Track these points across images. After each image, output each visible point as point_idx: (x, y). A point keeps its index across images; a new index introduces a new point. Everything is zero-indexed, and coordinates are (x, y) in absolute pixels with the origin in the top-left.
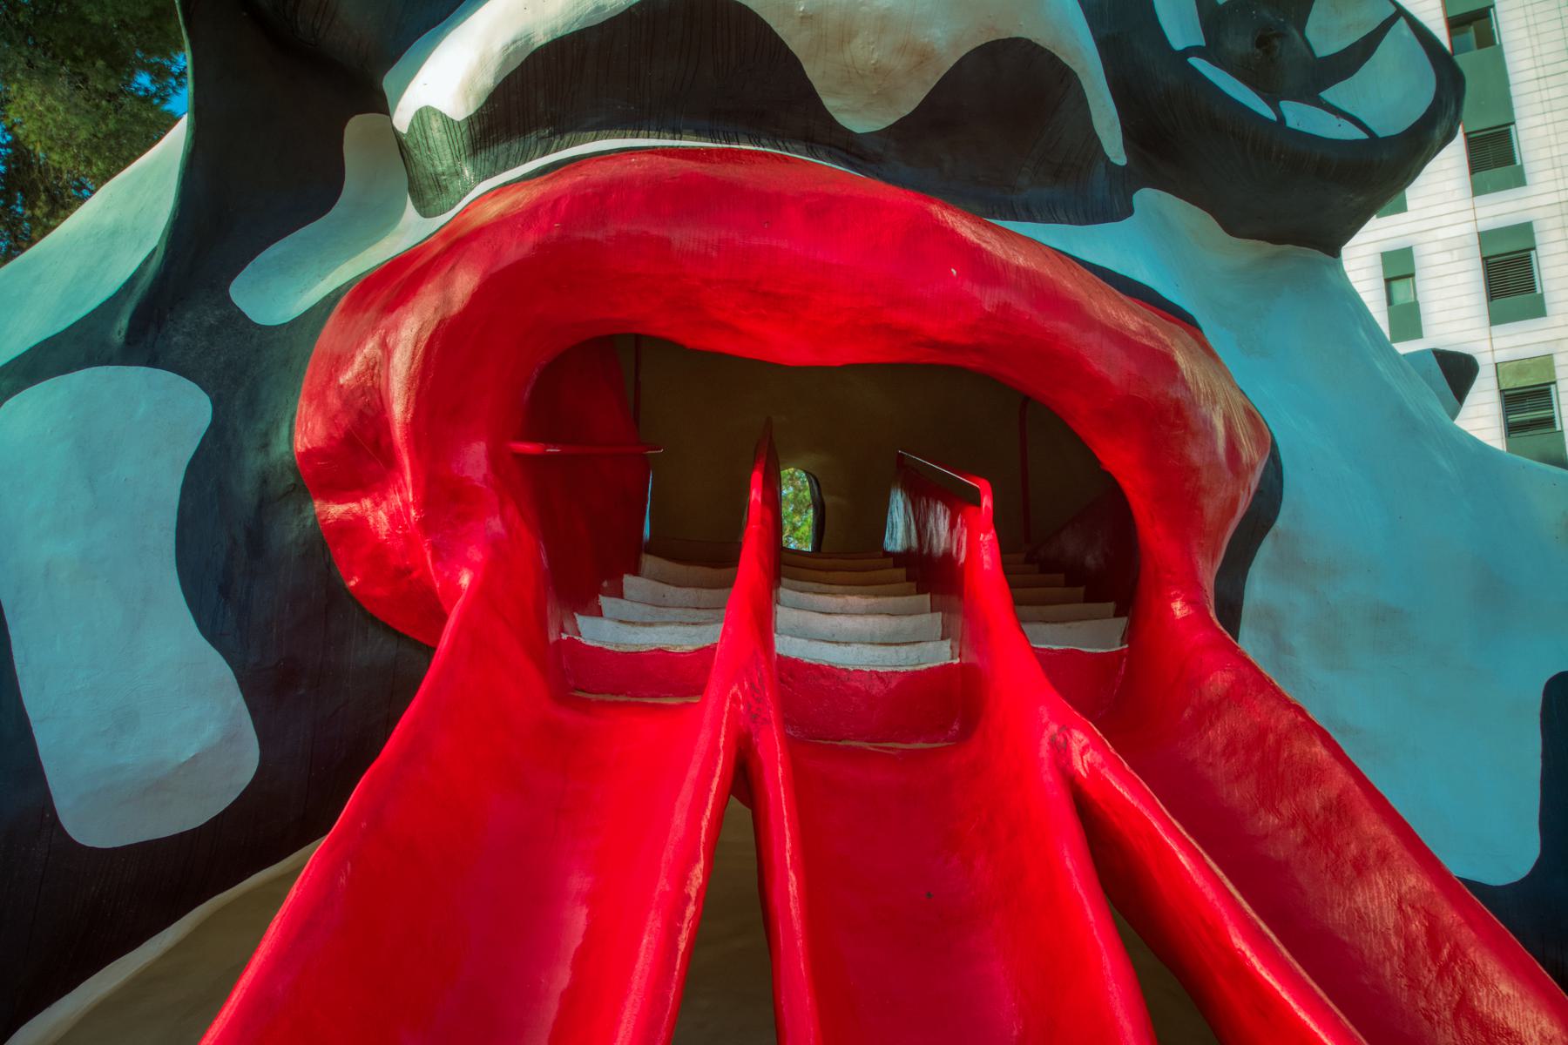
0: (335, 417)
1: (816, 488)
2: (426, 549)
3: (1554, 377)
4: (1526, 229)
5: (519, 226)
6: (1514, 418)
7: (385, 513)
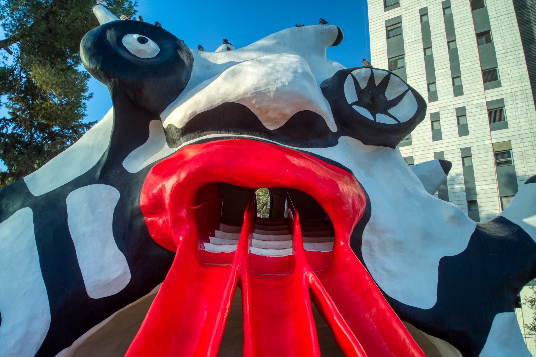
1: (270, 193)
3: (511, 147)
4: (502, 101)
6: (499, 161)
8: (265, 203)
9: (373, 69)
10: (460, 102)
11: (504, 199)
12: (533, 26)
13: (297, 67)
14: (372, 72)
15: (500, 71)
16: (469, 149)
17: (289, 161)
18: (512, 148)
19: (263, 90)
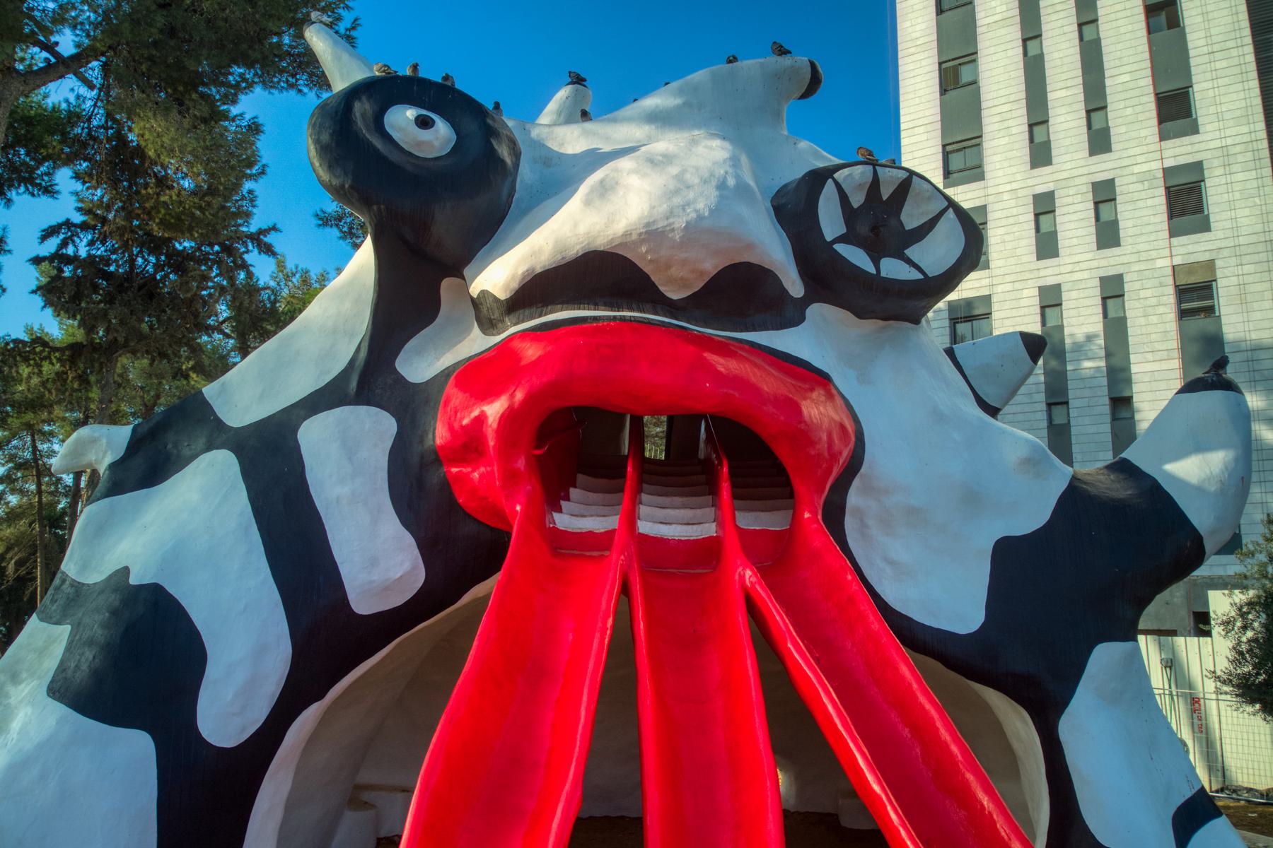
3: (1215, 276)
6: (1185, 306)
9: (876, 167)
10: (1102, 167)
13: (726, 173)
14: (875, 172)
16: (1119, 279)
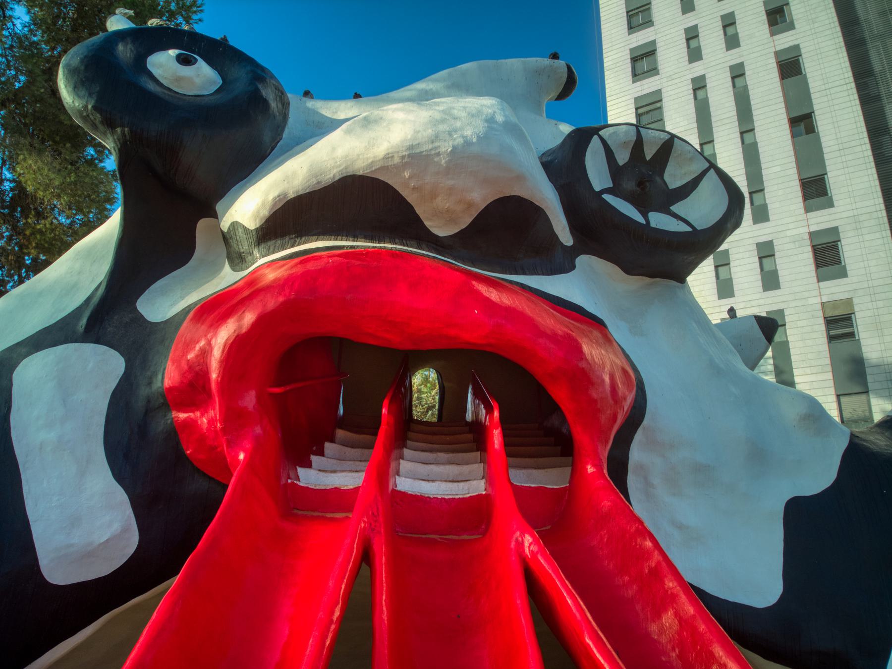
0: (185, 373)
2: (223, 442)
3: (854, 310)
4: (835, 230)
5: (276, 293)
6: (833, 333)
7: (206, 419)
8: (430, 405)
9: (640, 128)
11: (843, 399)
12: (886, 106)
15: (831, 181)
17: (479, 293)
18: (856, 310)
19: (424, 150)
